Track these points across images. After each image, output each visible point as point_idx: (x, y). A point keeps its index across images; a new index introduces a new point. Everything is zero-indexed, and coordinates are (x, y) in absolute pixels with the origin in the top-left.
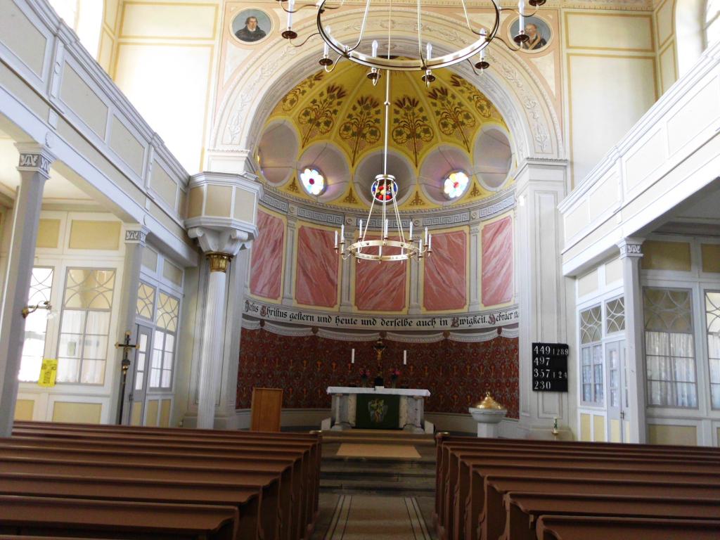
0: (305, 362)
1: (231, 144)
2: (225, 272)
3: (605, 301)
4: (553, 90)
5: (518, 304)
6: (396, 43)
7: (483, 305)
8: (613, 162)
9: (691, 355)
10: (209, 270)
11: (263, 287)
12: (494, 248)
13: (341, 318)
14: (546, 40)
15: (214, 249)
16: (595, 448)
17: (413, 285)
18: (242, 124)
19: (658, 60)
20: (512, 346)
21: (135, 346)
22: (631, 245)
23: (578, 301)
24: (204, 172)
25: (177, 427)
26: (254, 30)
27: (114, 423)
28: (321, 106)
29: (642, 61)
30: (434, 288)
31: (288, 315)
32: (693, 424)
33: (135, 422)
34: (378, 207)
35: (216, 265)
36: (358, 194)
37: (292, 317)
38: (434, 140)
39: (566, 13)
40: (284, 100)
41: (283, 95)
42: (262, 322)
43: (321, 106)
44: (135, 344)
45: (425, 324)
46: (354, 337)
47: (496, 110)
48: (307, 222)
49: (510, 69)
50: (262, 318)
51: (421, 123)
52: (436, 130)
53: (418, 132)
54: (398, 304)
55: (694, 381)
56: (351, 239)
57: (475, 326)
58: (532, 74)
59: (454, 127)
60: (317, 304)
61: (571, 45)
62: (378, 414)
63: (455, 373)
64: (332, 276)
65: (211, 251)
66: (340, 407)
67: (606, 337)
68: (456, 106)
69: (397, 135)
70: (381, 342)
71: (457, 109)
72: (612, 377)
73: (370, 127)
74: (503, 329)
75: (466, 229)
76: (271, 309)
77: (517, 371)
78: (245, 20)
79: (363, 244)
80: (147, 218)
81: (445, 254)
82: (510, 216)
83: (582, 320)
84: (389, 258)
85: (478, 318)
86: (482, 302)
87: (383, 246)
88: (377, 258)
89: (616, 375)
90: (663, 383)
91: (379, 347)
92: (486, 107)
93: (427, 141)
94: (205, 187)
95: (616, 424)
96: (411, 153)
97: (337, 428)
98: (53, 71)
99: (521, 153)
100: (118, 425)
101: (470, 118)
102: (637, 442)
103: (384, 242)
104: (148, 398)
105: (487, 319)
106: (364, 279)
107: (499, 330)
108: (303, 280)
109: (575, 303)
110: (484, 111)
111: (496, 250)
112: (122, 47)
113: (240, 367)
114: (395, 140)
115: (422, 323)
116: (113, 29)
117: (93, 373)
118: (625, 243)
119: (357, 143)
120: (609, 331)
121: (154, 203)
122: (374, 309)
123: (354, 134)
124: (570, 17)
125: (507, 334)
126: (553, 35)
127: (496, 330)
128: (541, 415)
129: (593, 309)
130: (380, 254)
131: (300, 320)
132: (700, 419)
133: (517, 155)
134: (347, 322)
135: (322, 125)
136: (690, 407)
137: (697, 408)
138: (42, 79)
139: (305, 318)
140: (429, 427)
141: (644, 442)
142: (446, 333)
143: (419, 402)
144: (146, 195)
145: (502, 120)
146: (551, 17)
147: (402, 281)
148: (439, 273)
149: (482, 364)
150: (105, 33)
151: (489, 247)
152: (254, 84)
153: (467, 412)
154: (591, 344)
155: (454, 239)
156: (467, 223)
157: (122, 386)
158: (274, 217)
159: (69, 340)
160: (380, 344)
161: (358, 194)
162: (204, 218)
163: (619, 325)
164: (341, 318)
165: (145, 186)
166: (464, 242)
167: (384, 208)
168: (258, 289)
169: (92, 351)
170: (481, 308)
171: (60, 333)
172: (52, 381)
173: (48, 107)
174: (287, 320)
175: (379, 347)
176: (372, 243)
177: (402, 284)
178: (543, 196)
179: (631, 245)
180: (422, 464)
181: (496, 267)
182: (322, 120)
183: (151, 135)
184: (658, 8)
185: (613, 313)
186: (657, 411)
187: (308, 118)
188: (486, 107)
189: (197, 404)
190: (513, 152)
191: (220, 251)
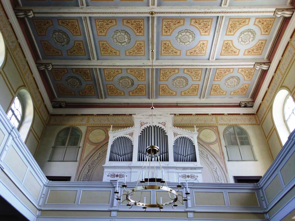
98: (4, 149)
116: (39, 137)
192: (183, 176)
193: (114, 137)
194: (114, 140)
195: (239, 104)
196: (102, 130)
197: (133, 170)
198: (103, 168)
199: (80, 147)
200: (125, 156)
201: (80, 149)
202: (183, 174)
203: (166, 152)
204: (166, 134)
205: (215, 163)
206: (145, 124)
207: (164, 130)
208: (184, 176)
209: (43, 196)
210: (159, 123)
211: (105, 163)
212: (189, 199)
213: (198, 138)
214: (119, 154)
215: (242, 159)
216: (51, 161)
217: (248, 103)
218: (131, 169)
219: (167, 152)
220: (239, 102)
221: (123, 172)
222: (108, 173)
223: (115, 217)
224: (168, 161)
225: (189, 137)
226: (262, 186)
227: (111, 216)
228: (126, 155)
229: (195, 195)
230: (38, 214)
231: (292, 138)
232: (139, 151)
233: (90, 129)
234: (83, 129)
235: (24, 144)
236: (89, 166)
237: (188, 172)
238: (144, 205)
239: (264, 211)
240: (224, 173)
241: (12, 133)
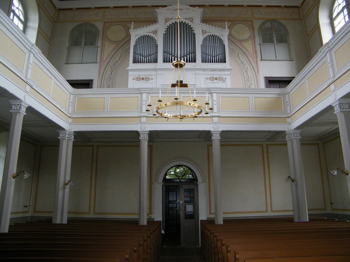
8: (324, 54)
80: (27, 96)
98: (28, 67)
138: (23, 72)
150: (40, 34)
165: (26, 77)
192: (210, 79)
193: (136, 36)
194: (137, 39)
196: (122, 25)
197: (159, 72)
198: (127, 72)
199: (98, 47)
200: (149, 57)
201: (99, 49)
202: (211, 76)
203: (193, 52)
204: (194, 32)
205: (246, 63)
206: (169, 19)
207: (191, 27)
208: (211, 79)
209: (71, 104)
210: (186, 19)
211: (129, 66)
212: (215, 104)
213: (230, 35)
214: (142, 55)
215: (276, 58)
216: (68, 64)
218: (157, 71)
219: (195, 52)
221: (149, 75)
222: (134, 76)
223: (145, 123)
224: (196, 62)
225: (219, 35)
226: (289, 91)
227: (141, 122)
228: (151, 56)
229: (221, 100)
230: (70, 122)
232: (164, 51)
233: (107, 25)
234: (100, 26)
236: (111, 67)
237: (216, 74)
238: (172, 116)
239: (287, 116)
240: (255, 74)
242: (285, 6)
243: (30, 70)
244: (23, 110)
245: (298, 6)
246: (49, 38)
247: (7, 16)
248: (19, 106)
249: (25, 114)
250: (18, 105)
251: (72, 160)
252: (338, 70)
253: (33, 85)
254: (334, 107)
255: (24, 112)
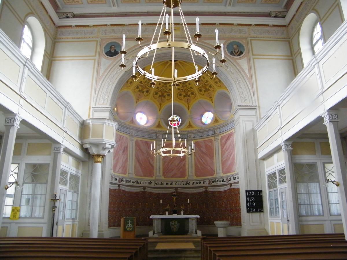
0: (140, 204)
1: (103, 104)
2: (101, 163)
3: (120, 228)
4: (248, 74)
5: (238, 173)
6: (177, 55)
7: (222, 174)
8: (312, 67)
9: (319, 192)
10: (94, 162)
11: (119, 169)
12: (226, 147)
13: (156, 182)
14: (243, 52)
15: (96, 153)
16: (286, 238)
17: (190, 166)
18: (108, 95)
19: (294, 60)
20: (234, 193)
21: (58, 199)
22: (286, 144)
23: (266, 170)
24: (91, 118)
25: (80, 237)
26: (114, 51)
27: (49, 236)
28: (144, 84)
29: (287, 61)
30: (200, 166)
31: (131, 181)
32: (322, 223)
33: (60, 235)
34: (170, 129)
35: (97, 160)
36: (163, 124)
37: (133, 183)
38: (196, 98)
39: (251, 40)
40: (127, 82)
41: (126, 81)
42: (119, 186)
43: (144, 84)
44: (59, 198)
45: (196, 183)
46: (163, 191)
47: (223, 83)
48: (139, 138)
49: (228, 66)
50: (119, 183)
51: (190, 90)
52: (197, 93)
53: (189, 94)
54: (183, 174)
55: (321, 203)
56: (159, 146)
57: (219, 184)
58: (238, 67)
59: (205, 91)
60: (145, 176)
61: (254, 54)
62: (175, 227)
63: (211, 206)
64: (152, 163)
65: (94, 154)
66: (157, 225)
67: (279, 186)
68: (205, 82)
69: (179, 96)
70: (175, 193)
71: (206, 83)
72: (283, 205)
73: (167, 92)
74: (232, 184)
75: (213, 138)
76: (123, 179)
77: (240, 204)
78: (109, 47)
79: (164, 150)
81: (204, 150)
82: (233, 132)
83: (279, 174)
84: (176, 155)
85: (220, 180)
86: (222, 172)
87: (173, 151)
88: (170, 155)
89: (285, 203)
90: (306, 205)
91: (174, 195)
92: (218, 82)
93: (193, 98)
94: (91, 125)
95: (285, 225)
96: (186, 104)
97: (156, 235)
98: (23, 81)
99: (235, 103)
100: (51, 237)
101: (212, 87)
102: (295, 233)
103: (174, 148)
104: (66, 223)
105: (225, 180)
106: (167, 163)
107: (231, 185)
108: (138, 165)
109: (264, 170)
110: (218, 84)
111: (227, 148)
112: (53, 62)
113: (109, 207)
114: (178, 98)
115: (194, 183)
116: (49, 54)
117: (38, 212)
118: (283, 144)
119: (161, 100)
120: (280, 183)
121: (68, 134)
122: (172, 177)
123: (160, 96)
124: (253, 41)
125: (234, 186)
126: (245, 51)
127: (229, 185)
128: (251, 224)
129: (273, 174)
130: (172, 154)
131: (137, 184)
132: (325, 221)
133: (234, 104)
134: (159, 184)
135: (145, 92)
136: (319, 215)
137: (323, 215)
139: (140, 183)
140: (199, 233)
141: (298, 234)
142: (206, 187)
143: (194, 221)
144: (64, 131)
145: (226, 88)
146: (244, 41)
147: (184, 164)
148: (201, 160)
149: (223, 201)
151: (224, 147)
152: (114, 76)
153: (214, 224)
154: (273, 190)
155: (208, 143)
156: (213, 135)
157: (53, 219)
158: (124, 136)
159: (26, 197)
160: (174, 194)
161: (163, 124)
162: (91, 139)
163: (285, 181)
164: (156, 182)
165: (63, 127)
166: (212, 144)
167: (173, 130)
168: (117, 170)
169: (38, 202)
170: (222, 175)
171: (22, 194)
172: (17, 216)
173: (20, 97)
174: (131, 184)
175: (174, 195)
176: (168, 149)
177: (185, 165)
178: (246, 122)
179: (286, 144)
180: (196, 251)
181: (228, 156)
182: (145, 90)
183: (66, 103)
184: (292, 37)
185: (281, 175)
186: (304, 218)
187: (138, 89)
188: (218, 82)
189: (89, 225)
190: (232, 102)
191: (99, 154)
195: (268, 14)
217: (280, 13)
220: (269, 12)
231: (310, 64)
235: (41, 73)
241: (27, 64)
242: (272, 25)
243: (65, 121)
244: (17, 123)
245: (285, 25)
246: (6, 4)
247: (18, 48)
248: (13, 119)
249: (19, 127)
250: (12, 118)
251: (14, 150)
252: (326, 81)
253: (26, 98)
254: (324, 118)
255: (18, 125)
